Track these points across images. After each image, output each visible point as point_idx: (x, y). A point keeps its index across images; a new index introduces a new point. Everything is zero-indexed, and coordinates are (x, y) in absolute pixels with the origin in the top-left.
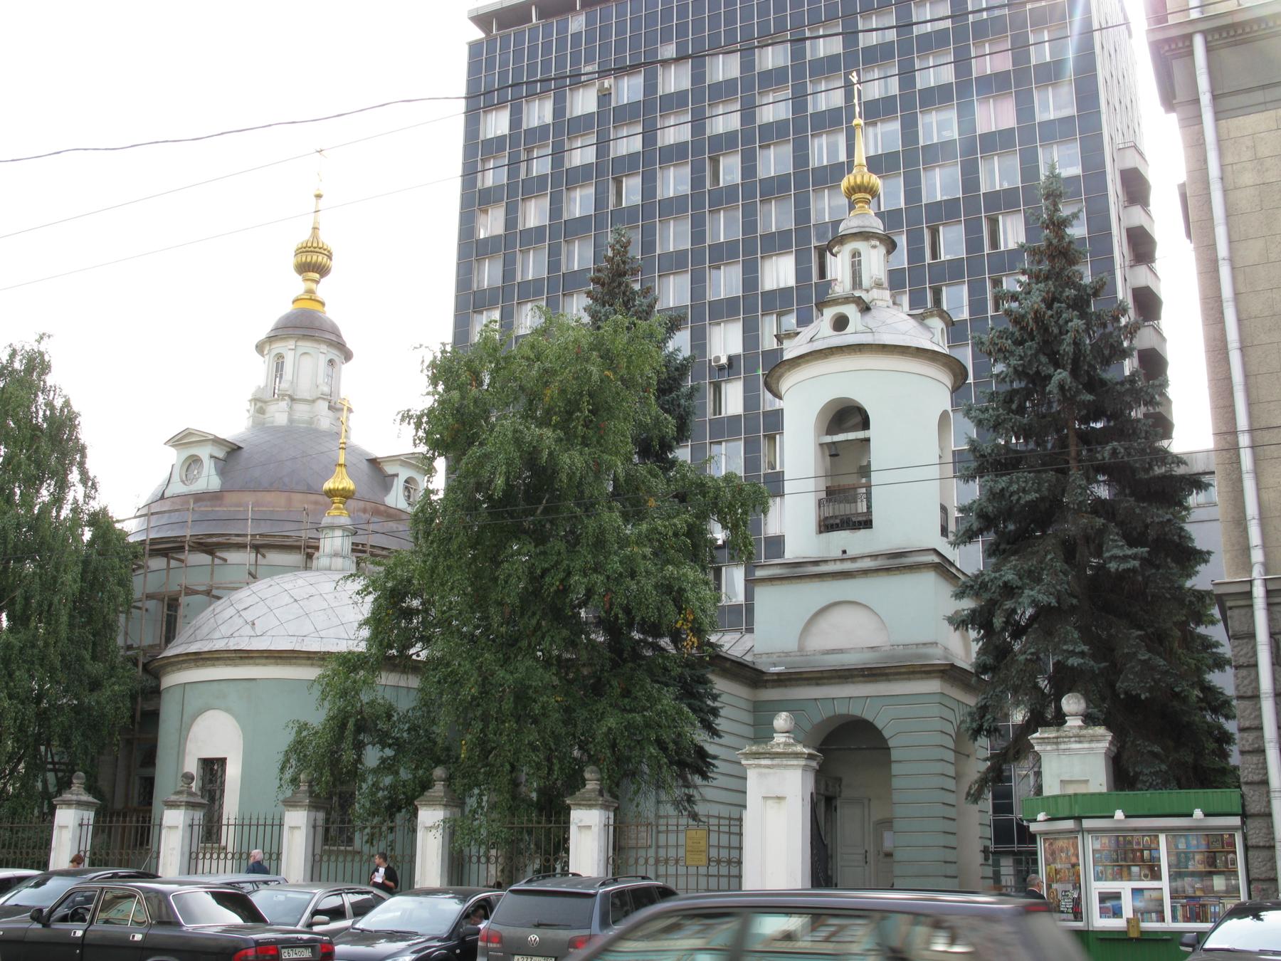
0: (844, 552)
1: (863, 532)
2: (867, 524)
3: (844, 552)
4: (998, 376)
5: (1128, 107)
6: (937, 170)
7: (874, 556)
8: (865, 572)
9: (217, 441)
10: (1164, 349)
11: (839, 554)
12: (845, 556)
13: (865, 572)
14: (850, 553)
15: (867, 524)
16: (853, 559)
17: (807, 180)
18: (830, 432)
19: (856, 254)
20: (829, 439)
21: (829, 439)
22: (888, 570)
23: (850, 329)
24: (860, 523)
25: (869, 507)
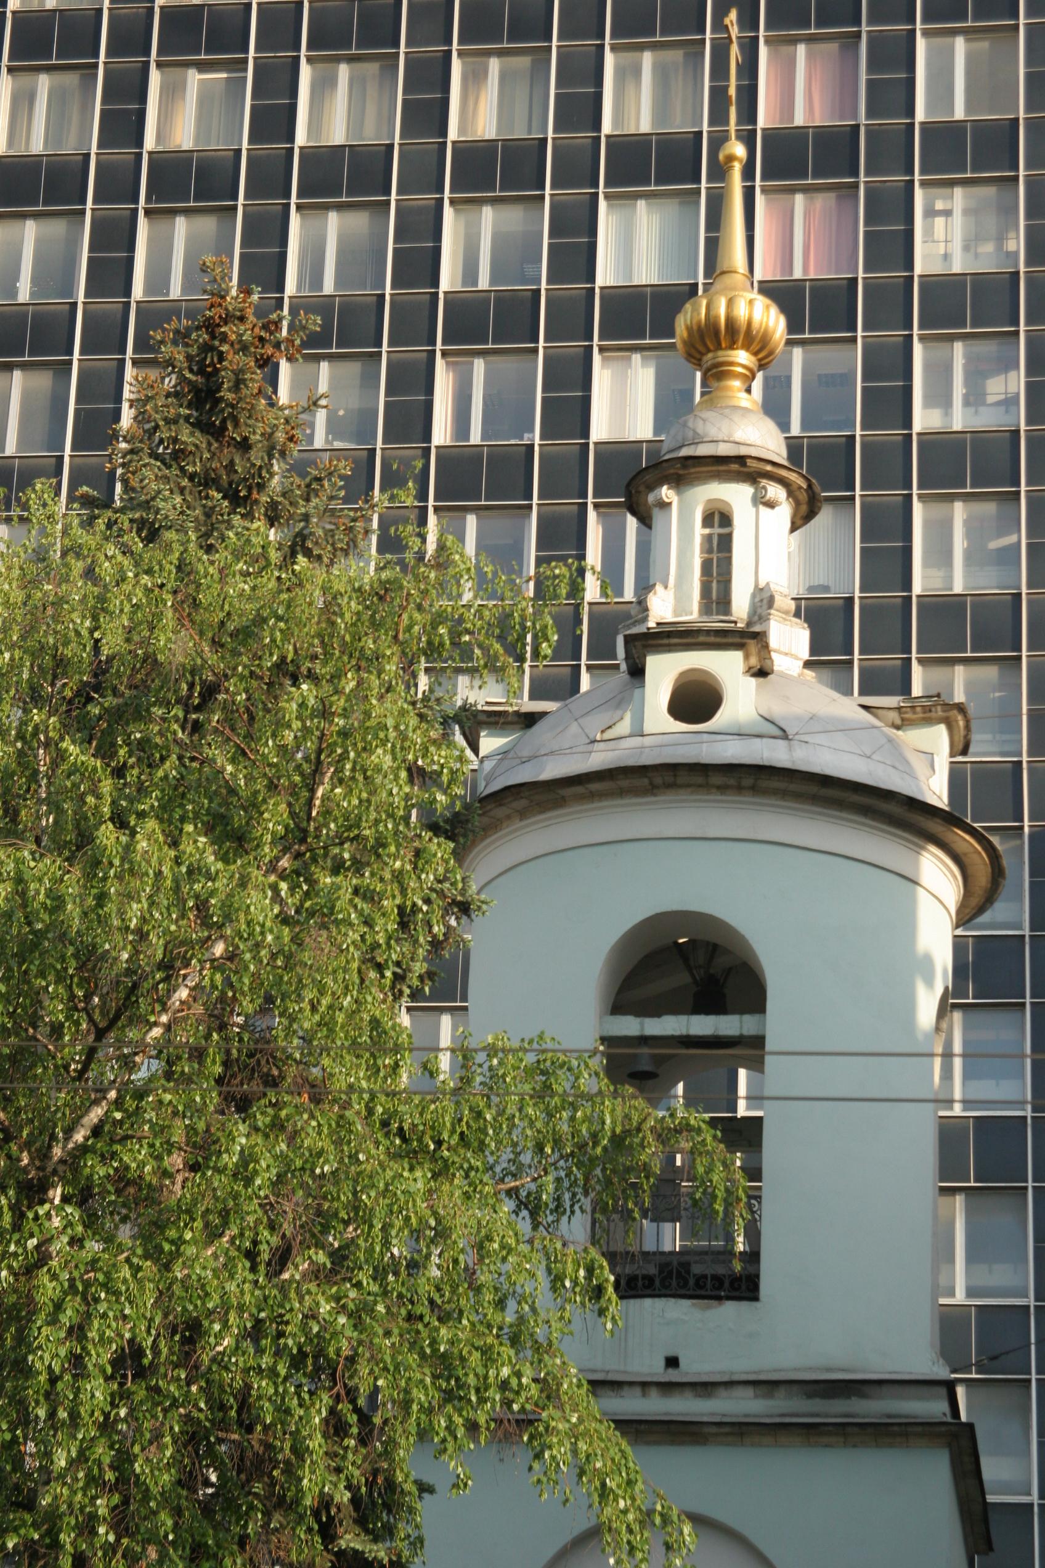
0: (672, 1362)
1: (730, 1308)
2: (744, 1286)
3: (672, 1362)
4: (254, 806)
5: (454, 253)
6: (17, 374)
7: (766, 1386)
8: (740, 1432)
9: (753, 1256)
10: (920, 790)
11: (655, 1369)
12: (673, 1376)
13: (740, 1432)
14: (693, 1368)
15: (744, 1286)
16: (705, 1388)
17: (559, 319)
18: (618, 1006)
19: (719, 519)
20: (629, 1026)
21: (629, 1026)
22: (811, 1432)
23: (722, 718)
24: (718, 1280)
25: (753, 1234)
